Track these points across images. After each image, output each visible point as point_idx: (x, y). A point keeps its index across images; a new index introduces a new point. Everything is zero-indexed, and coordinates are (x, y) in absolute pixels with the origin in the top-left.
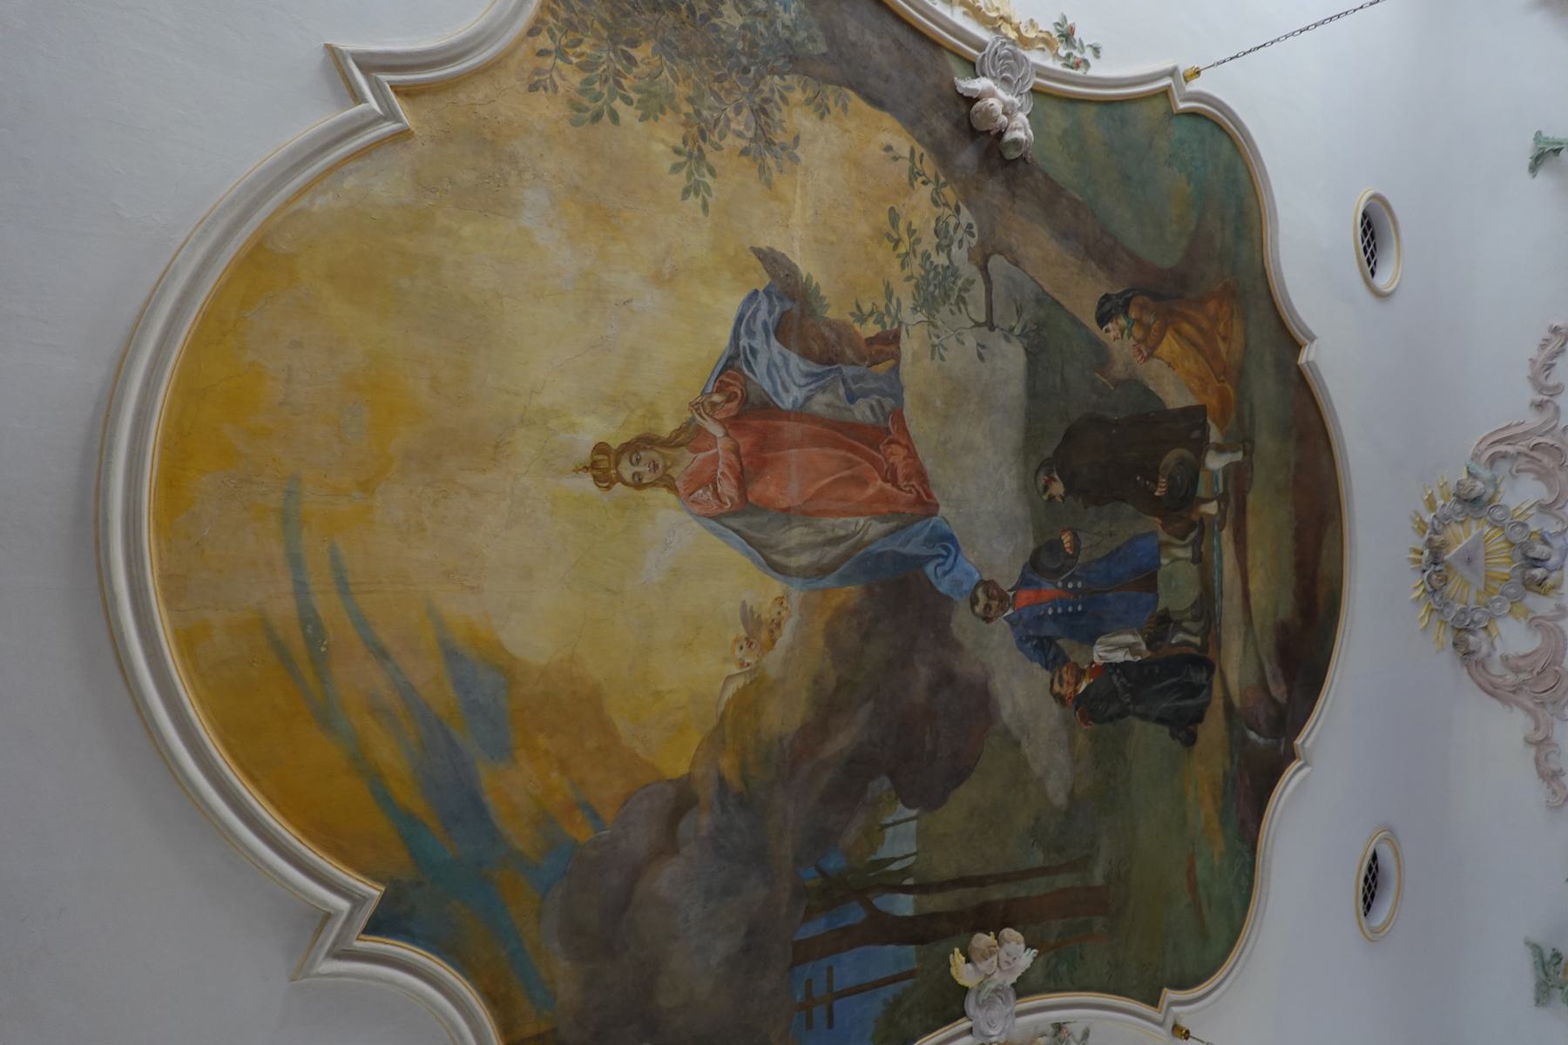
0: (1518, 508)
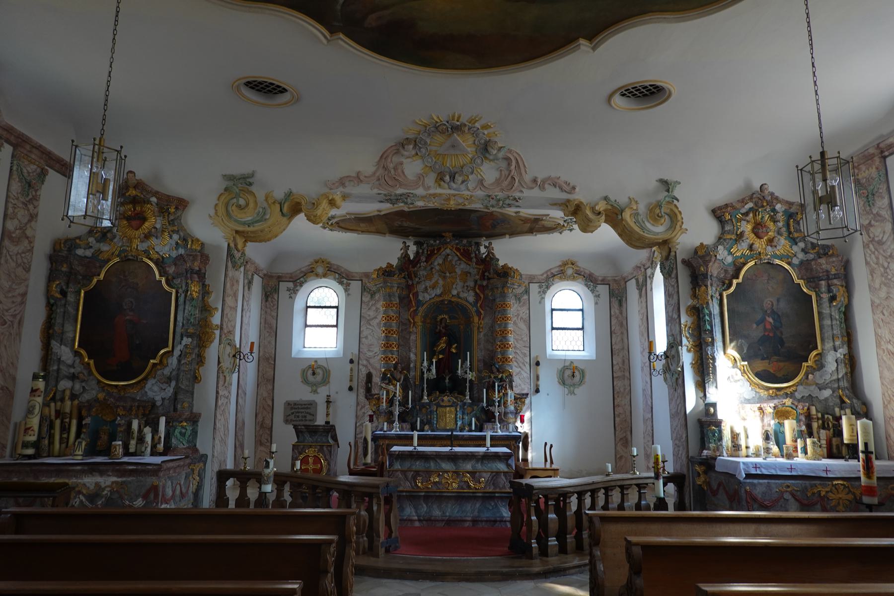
0: (481, 171)
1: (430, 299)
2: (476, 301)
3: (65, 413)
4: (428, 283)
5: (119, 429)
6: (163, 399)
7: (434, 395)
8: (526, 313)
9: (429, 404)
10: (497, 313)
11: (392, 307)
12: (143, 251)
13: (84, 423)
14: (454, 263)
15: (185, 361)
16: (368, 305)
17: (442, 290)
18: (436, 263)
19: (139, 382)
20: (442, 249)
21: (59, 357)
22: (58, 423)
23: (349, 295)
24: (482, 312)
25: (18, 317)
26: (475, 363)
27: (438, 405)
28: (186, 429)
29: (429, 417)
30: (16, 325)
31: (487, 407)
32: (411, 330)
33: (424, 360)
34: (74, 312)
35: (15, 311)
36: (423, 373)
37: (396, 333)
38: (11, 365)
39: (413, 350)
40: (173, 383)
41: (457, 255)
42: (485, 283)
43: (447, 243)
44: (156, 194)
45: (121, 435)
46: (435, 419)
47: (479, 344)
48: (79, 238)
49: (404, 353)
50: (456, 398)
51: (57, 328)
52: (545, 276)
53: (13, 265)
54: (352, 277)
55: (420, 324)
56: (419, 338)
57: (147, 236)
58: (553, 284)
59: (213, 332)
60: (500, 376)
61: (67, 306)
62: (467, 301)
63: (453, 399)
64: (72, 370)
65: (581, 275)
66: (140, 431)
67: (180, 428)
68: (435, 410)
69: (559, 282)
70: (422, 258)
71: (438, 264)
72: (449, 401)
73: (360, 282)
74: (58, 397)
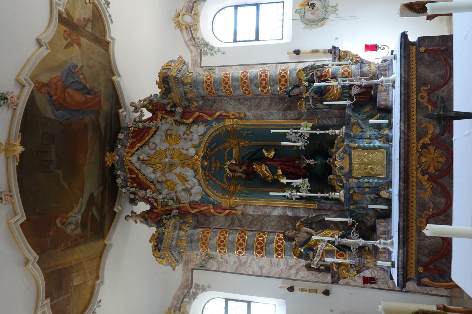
1: (200, 185)
2: (205, 122)
4: (180, 187)
7: (334, 183)
8: (236, 69)
9: (348, 190)
10: (220, 93)
11: (206, 239)
14: (153, 152)
16: (222, 263)
17: (188, 169)
18: (152, 176)
20: (131, 166)
23: (209, 287)
24: (218, 113)
26: (289, 122)
27: (349, 175)
29: (367, 190)
31: (351, 98)
32: (240, 213)
33: (285, 196)
36: (302, 198)
37: (242, 234)
39: (268, 210)
41: (141, 147)
42: (179, 110)
43: (122, 160)
46: (371, 181)
47: (262, 118)
49: (273, 223)
50: (338, 149)
52: (192, 48)
55: (233, 200)
56: (248, 202)
58: (202, 39)
60: (306, 84)
62: (204, 135)
63: (339, 152)
65: (193, 7)
68: (356, 181)
69: (201, 32)
70: (141, 195)
71: (154, 172)
72: (342, 158)
73: (194, 271)
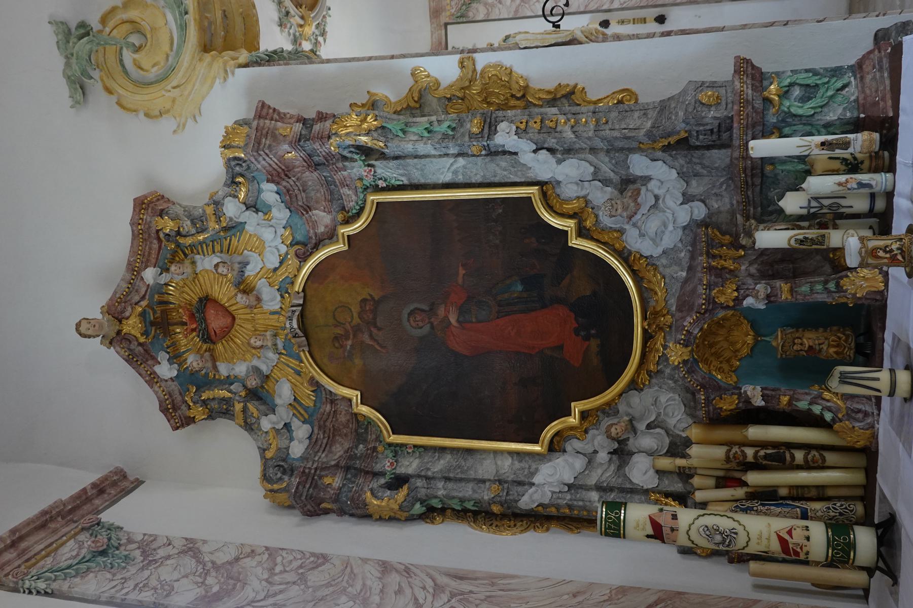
3: (728, 459)
5: (785, 296)
6: (687, 199)
12: (282, 297)
13: (759, 402)
15: (567, 128)
19: (634, 273)
21: (566, 489)
22: (755, 478)
25: (443, 580)
28: (791, 85)
30: (465, 586)
34: (448, 457)
35: (424, 588)
38: (580, 599)
40: (639, 164)
44: (134, 270)
45: (805, 289)
48: (263, 451)
51: (486, 495)
53: (295, 591)
54: (440, 43)
57: (244, 287)
59: (483, 72)
61: (430, 473)
64: (603, 456)
66: (794, 222)
67: (787, 103)
73: (449, 27)
74: (678, 486)
